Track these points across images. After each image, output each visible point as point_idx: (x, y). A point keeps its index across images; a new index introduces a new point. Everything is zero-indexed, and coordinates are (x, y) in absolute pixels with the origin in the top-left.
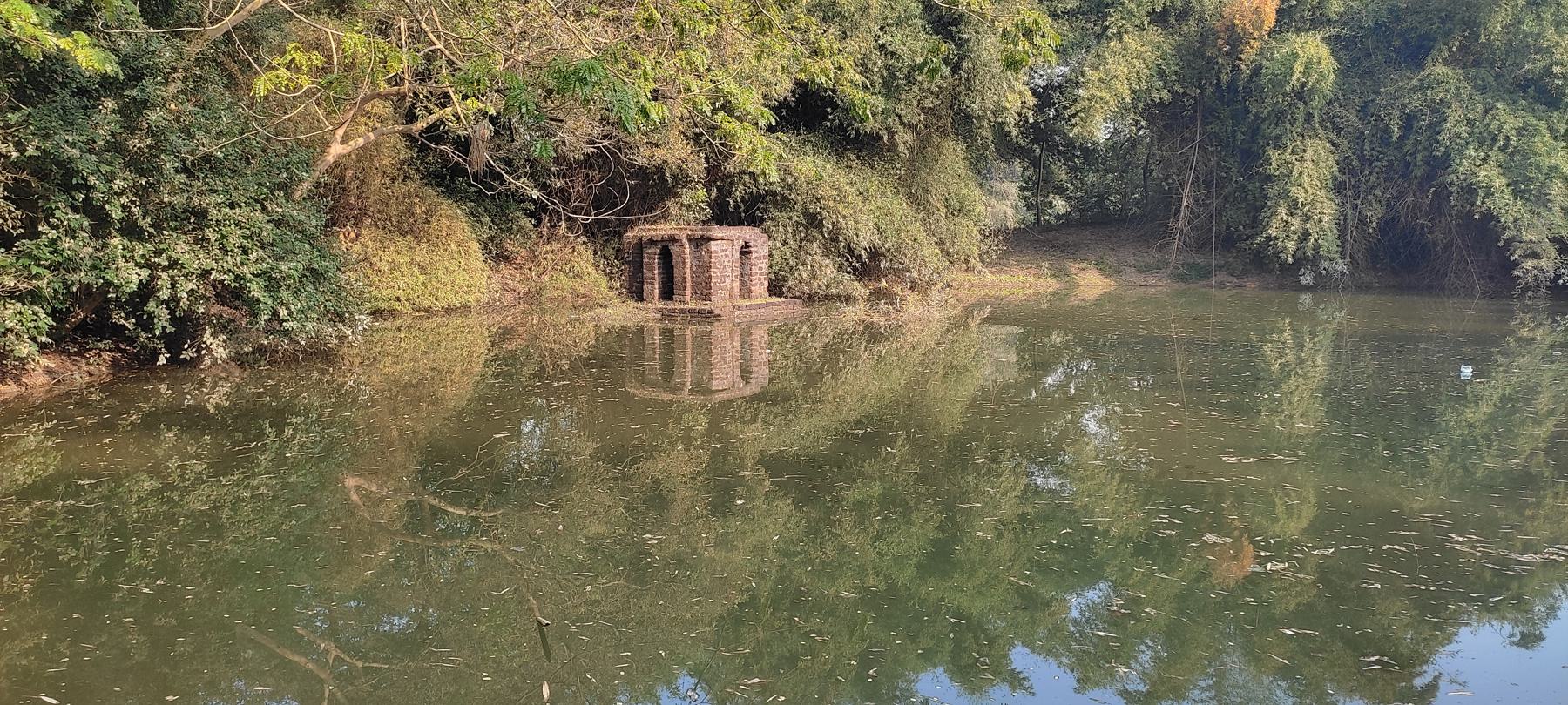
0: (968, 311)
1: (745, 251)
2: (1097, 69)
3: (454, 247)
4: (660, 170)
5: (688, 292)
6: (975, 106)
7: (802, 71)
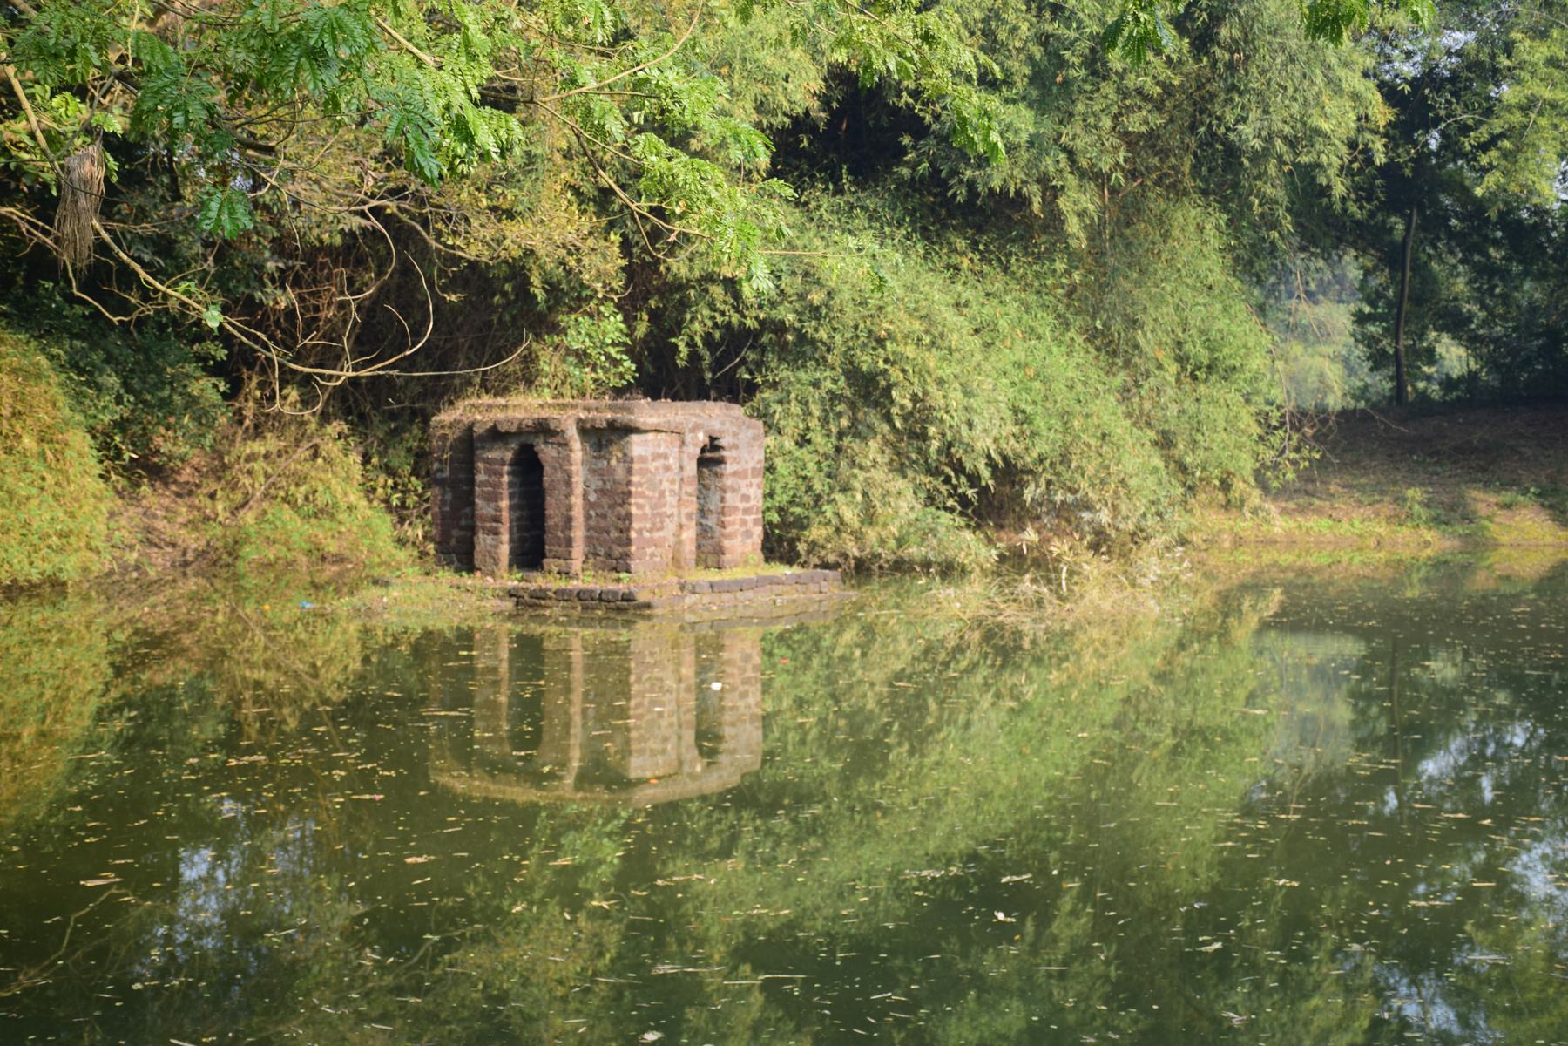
0: (1228, 604)
1: (710, 458)
2: (1543, 35)
3: (28, 442)
4: (517, 272)
5: (578, 551)
6: (1246, 130)
7: (841, 42)
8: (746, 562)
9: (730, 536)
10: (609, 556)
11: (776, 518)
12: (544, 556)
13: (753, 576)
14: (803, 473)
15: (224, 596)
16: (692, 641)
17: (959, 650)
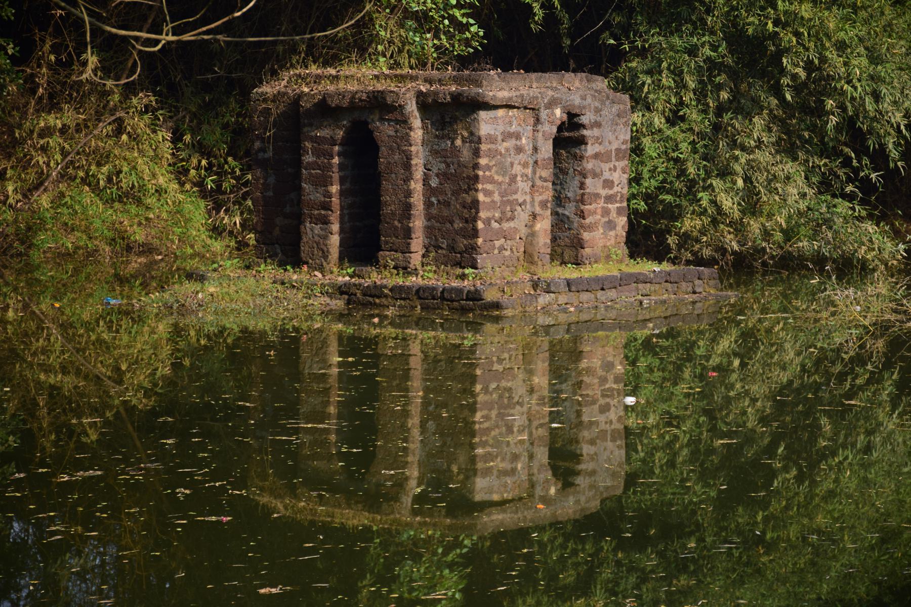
1: (569, 138)
5: (418, 243)
8: (608, 257)
9: (590, 228)
10: (452, 249)
11: (642, 206)
12: (380, 249)
13: (616, 273)
14: (675, 155)
15: (15, 289)
16: (546, 346)
17: (860, 360)
